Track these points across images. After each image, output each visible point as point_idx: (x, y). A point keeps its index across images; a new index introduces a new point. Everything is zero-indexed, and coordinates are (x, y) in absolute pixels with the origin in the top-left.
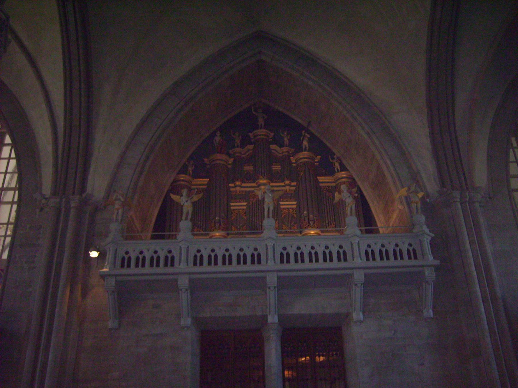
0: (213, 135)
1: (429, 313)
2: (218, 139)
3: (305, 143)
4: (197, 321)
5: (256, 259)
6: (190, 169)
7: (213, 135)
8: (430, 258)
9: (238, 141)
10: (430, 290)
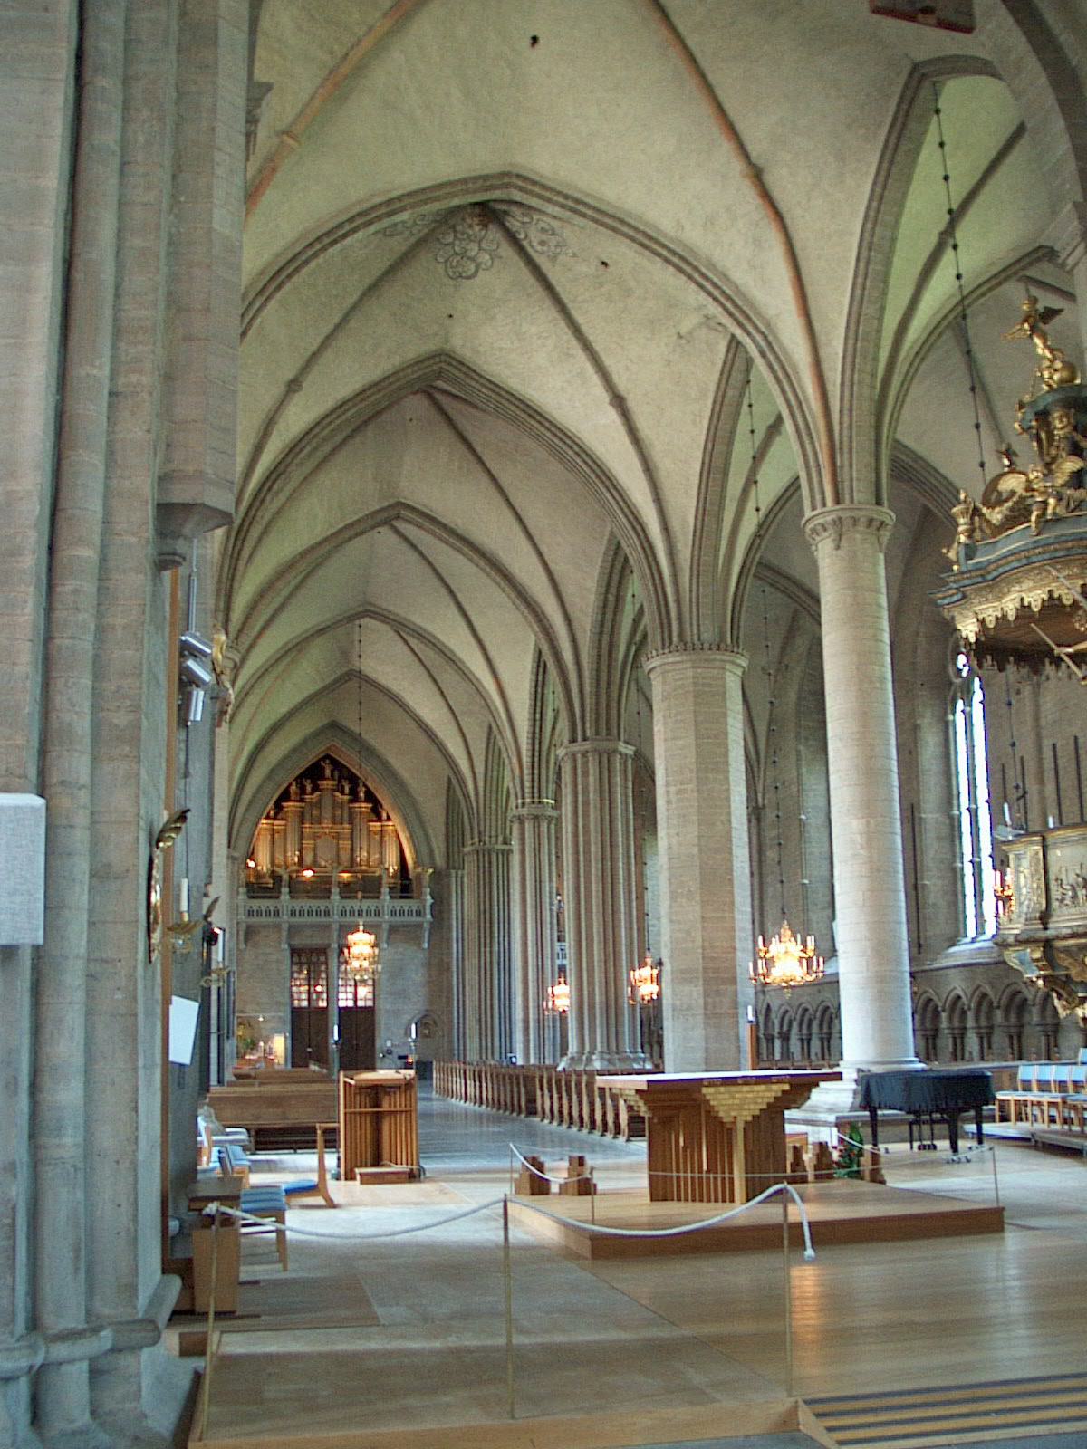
0: (290, 785)
1: (426, 945)
2: (293, 787)
3: (362, 795)
4: (290, 945)
5: (327, 913)
6: (272, 813)
7: (290, 785)
8: (429, 916)
9: (309, 788)
10: (426, 934)
